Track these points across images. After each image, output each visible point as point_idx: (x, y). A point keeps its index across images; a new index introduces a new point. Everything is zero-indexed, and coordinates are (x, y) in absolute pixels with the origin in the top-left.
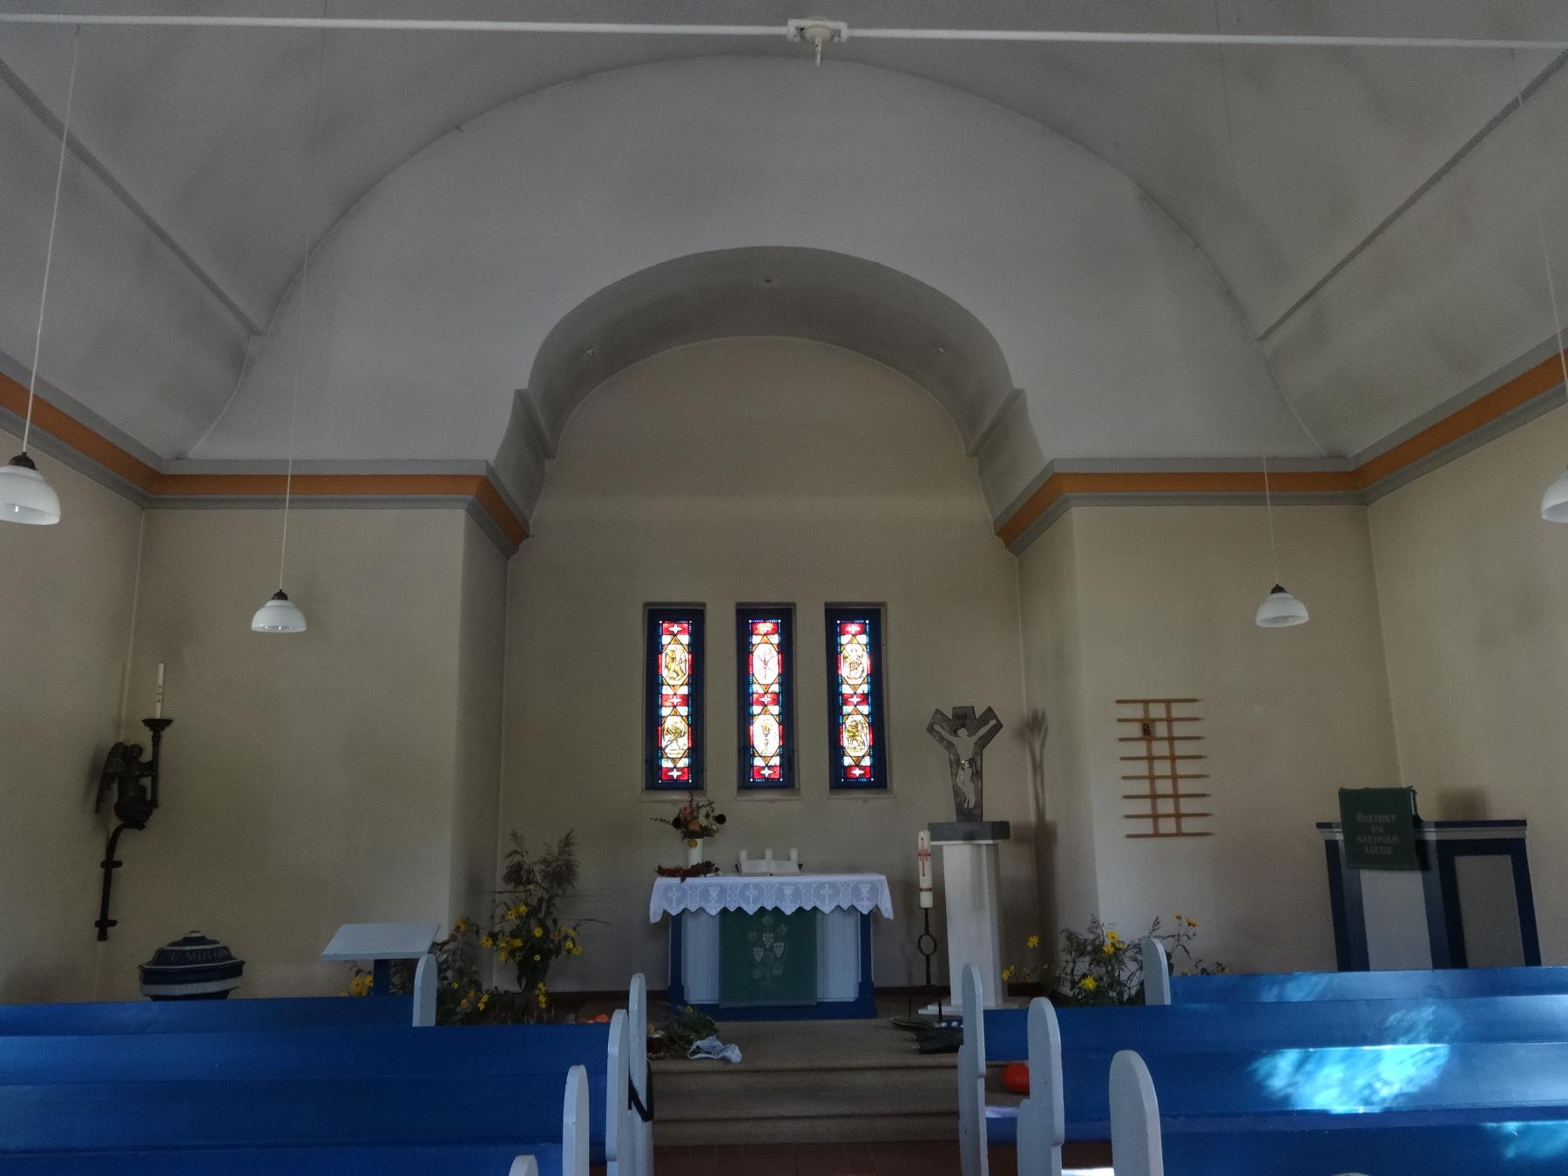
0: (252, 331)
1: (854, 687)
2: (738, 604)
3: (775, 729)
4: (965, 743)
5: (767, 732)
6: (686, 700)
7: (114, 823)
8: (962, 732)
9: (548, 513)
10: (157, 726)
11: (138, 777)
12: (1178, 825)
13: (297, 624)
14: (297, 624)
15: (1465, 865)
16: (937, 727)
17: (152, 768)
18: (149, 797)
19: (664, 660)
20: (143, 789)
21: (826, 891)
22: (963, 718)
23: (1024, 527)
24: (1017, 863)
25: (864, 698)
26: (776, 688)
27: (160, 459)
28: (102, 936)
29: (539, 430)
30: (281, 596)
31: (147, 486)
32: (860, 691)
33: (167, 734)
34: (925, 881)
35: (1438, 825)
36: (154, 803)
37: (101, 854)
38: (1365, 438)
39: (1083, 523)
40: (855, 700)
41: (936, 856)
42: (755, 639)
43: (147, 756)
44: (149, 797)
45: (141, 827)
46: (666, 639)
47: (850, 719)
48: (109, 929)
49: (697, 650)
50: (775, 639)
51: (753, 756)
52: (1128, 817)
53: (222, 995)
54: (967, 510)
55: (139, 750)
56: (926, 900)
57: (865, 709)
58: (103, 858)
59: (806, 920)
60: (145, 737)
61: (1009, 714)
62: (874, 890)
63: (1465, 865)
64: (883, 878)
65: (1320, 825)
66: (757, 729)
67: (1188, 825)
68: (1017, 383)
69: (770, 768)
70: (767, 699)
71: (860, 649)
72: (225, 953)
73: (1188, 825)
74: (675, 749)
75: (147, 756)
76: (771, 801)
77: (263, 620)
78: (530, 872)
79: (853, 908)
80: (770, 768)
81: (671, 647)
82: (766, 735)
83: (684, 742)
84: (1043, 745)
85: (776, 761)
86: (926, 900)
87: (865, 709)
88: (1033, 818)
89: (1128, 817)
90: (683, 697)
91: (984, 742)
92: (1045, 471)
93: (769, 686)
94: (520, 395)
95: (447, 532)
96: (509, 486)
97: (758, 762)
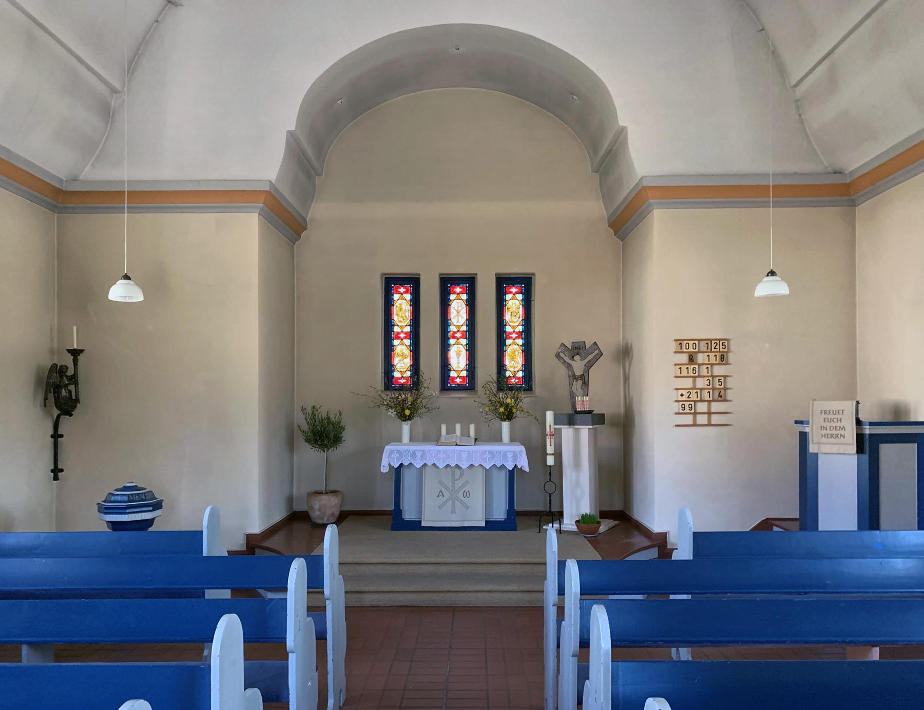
0: (114, 91)
1: (513, 327)
2: (441, 274)
3: (464, 354)
4: (578, 366)
5: (458, 354)
6: (408, 335)
7: (56, 412)
8: (577, 358)
9: (321, 211)
10: (75, 353)
11: (67, 385)
12: (709, 419)
13: (137, 296)
14: (137, 296)
15: (886, 450)
16: (562, 355)
17: (74, 379)
18: (74, 397)
19: (395, 310)
20: (70, 392)
21: (488, 456)
22: (577, 349)
23: (625, 222)
24: (610, 438)
25: (519, 335)
26: (464, 328)
27: (61, 180)
28: (56, 478)
29: (311, 155)
30: (127, 277)
31: (61, 200)
32: (517, 330)
33: (81, 358)
34: (550, 449)
35: (871, 424)
36: (77, 400)
37: (51, 431)
38: (858, 159)
39: (661, 223)
40: (514, 335)
41: (557, 434)
42: (452, 297)
43: (70, 372)
44: (74, 397)
45: (71, 415)
46: (396, 297)
47: (511, 347)
48: (60, 474)
49: (415, 303)
50: (464, 297)
51: (450, 370)
52: (676, 414)
53: (150, 522)
54: (592, 209)
55: (62, 370)
56: (550, 461)
57: (520, 342)
58: (52, 433)
59: (285, 589)
60: (68, 360)
61: (607, 345)
62: (515, 456)
63: (886, 450)
64: (523, 448)
65: (796, 422)
66: (452, 353)
67: (715, 419)
68: (622, 122)
69: (460, 377)
70: (458, 335)
71: (517, 303)
72: (151, 495)
73: (715, 419)
74: (402, 364)
75: (70, 372)
76: (460, 398)
77: (119, 292)
78: (329, 434)
79: (503, 466)
80: (460, 377)
81: (399, 302)
82: (458, 359)
83: (408, 362)
84: (630, 365)
85: (464, 374)
86: (550, 461)
87: (520, 342)
88: (622, 411)
89: (676, 414)
90: (406, 333)
91: (589, 366)
92: (637, 185)
93: (512, 299)
94: (290, 134)
95: (246, 232)
96: (288, 194)
97: (453, 374)
